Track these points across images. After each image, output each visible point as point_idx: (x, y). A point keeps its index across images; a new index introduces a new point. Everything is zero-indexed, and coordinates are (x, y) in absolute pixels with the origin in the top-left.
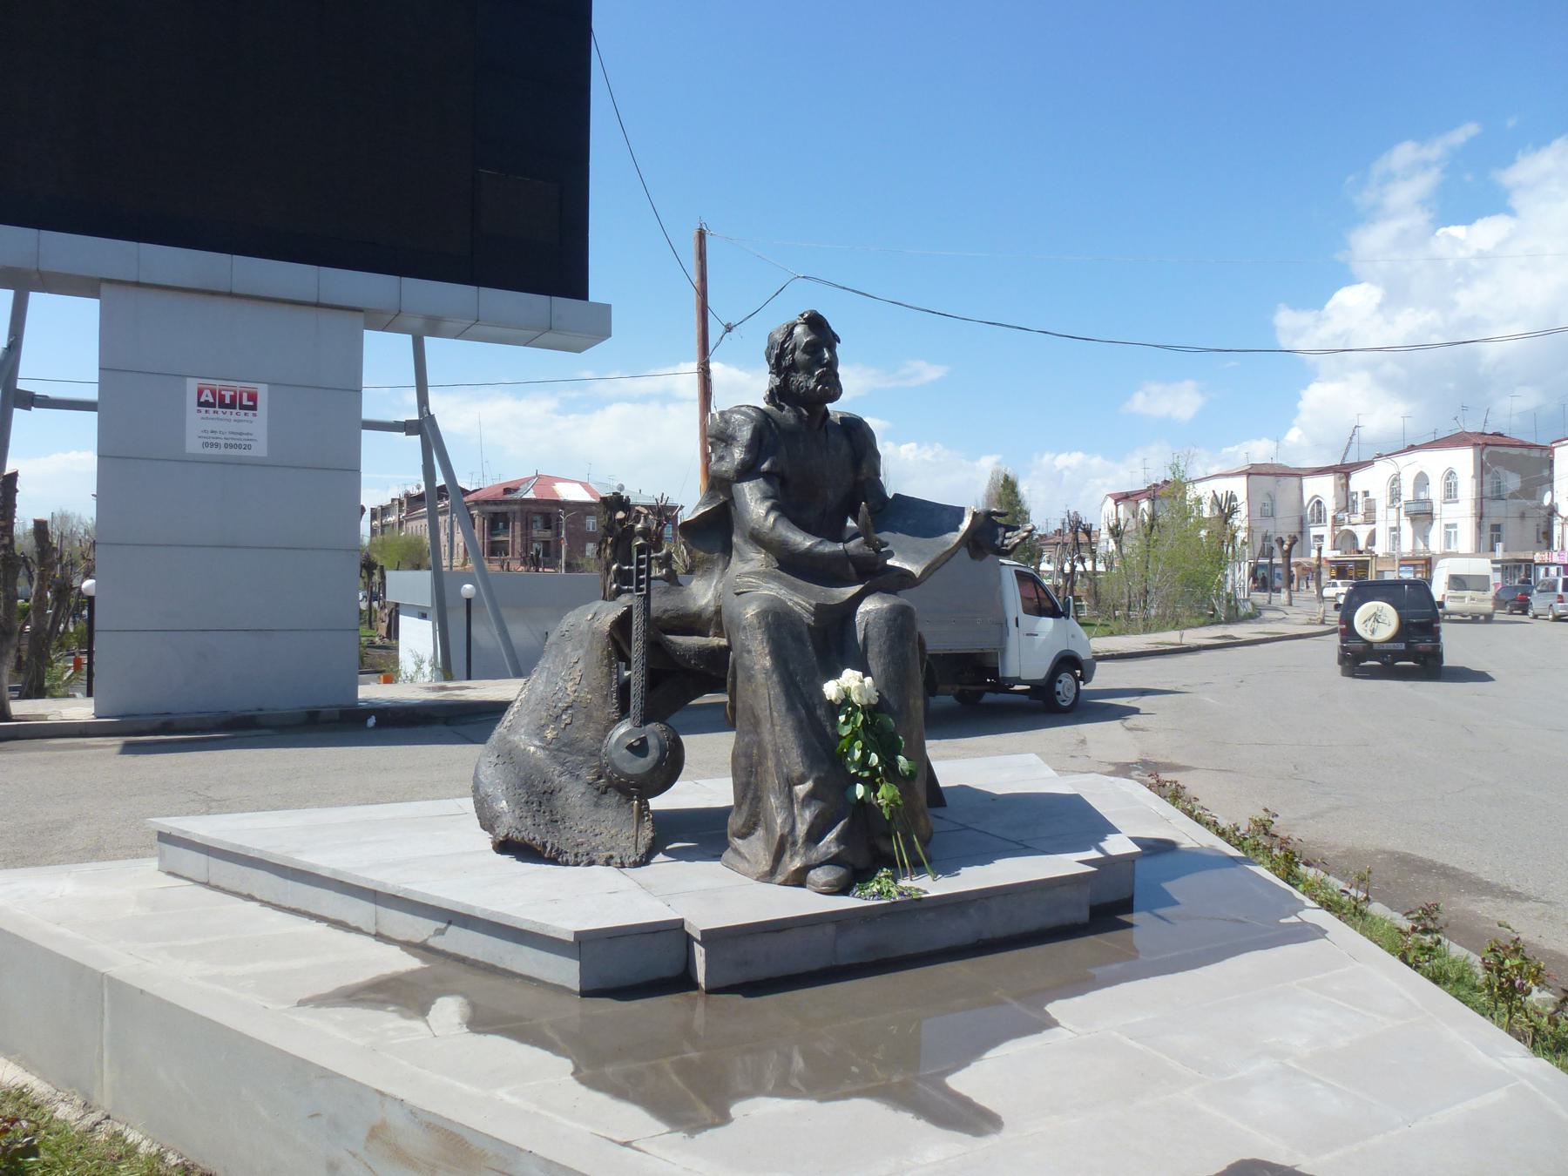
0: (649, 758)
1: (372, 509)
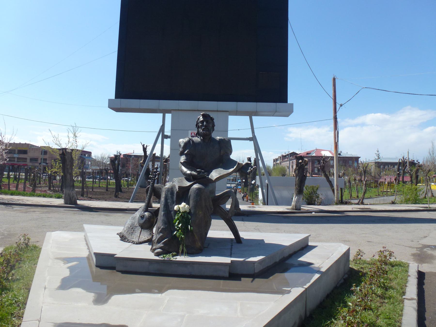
1: (274, 159)
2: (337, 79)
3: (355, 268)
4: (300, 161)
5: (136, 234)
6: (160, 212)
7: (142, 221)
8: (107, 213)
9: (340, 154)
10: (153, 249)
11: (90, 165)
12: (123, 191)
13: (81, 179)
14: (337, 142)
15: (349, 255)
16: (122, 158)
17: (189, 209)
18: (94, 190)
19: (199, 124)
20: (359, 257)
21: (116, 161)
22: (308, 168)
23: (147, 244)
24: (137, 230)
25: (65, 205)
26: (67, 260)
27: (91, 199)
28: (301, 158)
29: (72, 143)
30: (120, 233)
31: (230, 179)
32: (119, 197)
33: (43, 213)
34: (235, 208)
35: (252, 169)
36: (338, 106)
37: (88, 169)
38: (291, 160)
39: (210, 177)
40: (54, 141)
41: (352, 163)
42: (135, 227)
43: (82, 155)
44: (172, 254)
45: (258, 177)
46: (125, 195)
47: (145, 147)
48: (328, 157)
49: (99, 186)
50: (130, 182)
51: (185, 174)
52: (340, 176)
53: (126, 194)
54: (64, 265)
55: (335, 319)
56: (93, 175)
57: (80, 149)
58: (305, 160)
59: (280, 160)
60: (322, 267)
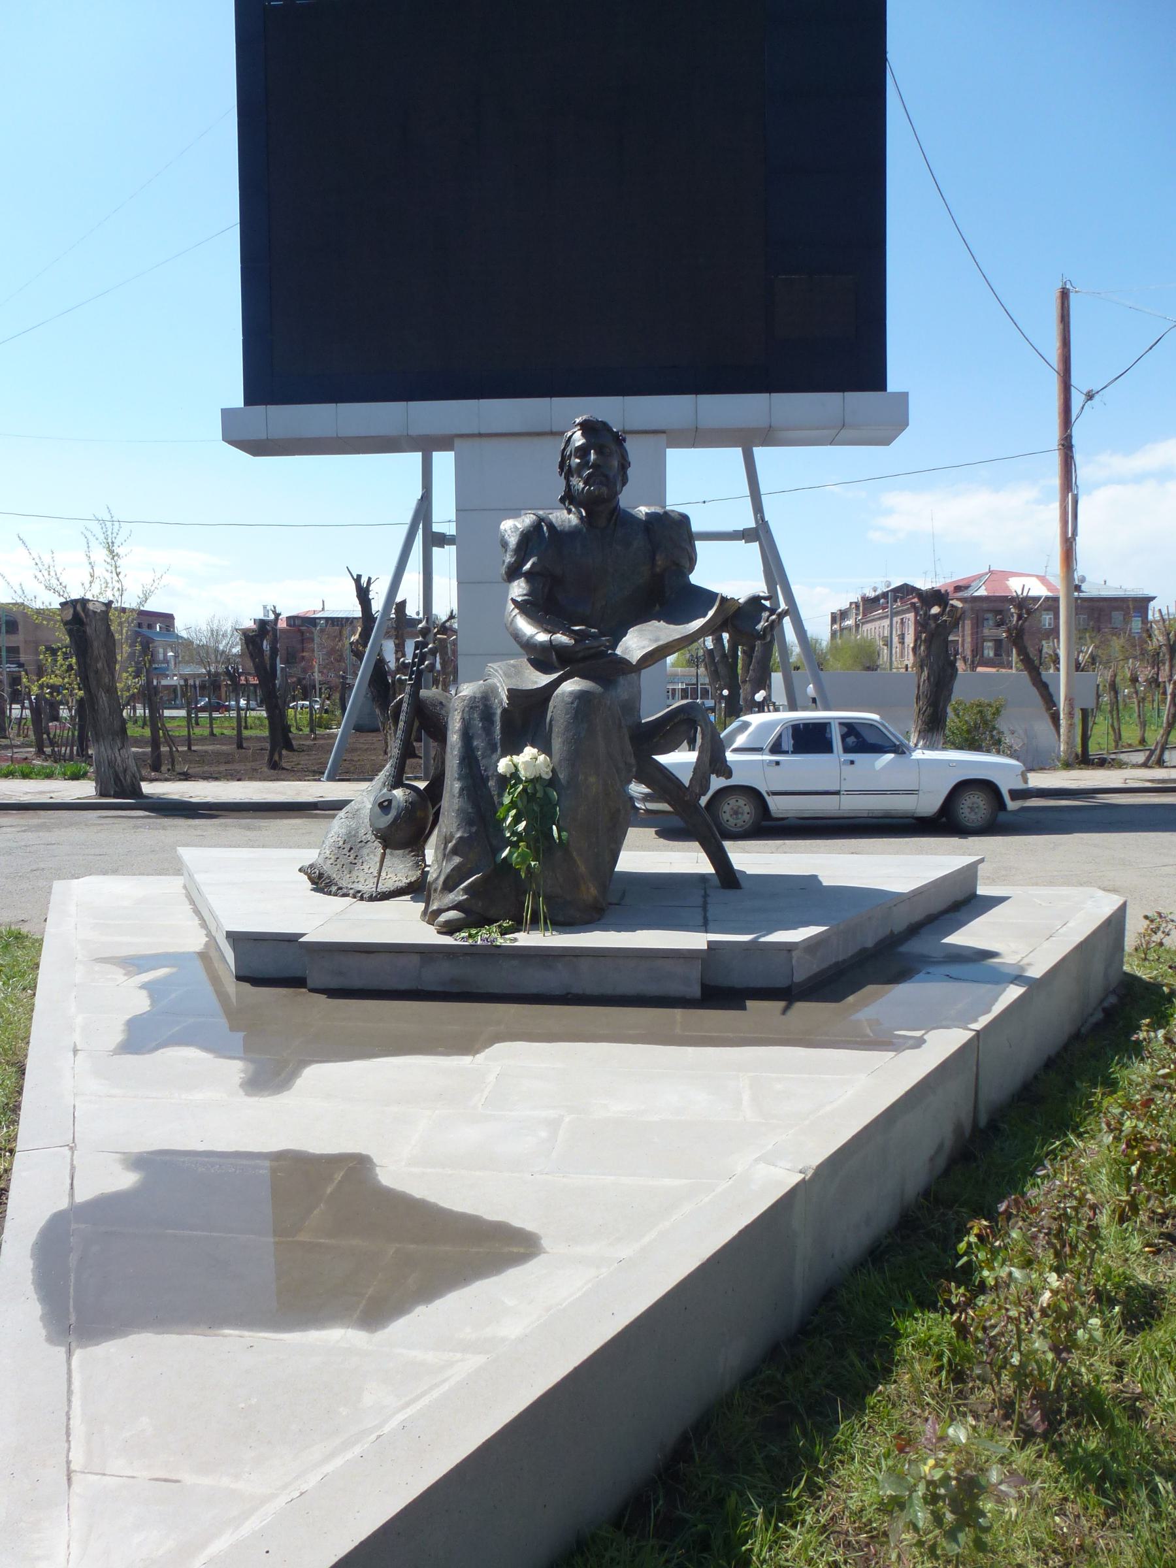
0: (390, 816)
1: (832, 613)
2: (1076, 292)
3: (1145, 974)
4: (935, 610)
5: (365, 867)
6: (447, 782)
7: (386, 820)
8: (248, 820)
9: (1078, 588)
10: (430, 910)
11: (173, 663)
12: (295, 747)
13: (147, 711)
14: (1070, 536)
15: (1124, 925)
16: (282, 630)
17: (549, 770)
18: (193, 748)
19: (573, 458)
20: (1156, 938)
21: (265, 643)
22: (960, 642)
23: (408, 897)
24: (368, 855)
25: (99, 799)
26: (134, 964)
27: (186, 777)
28: (937, 597)
29: (103, 581)
30: (311, 866)
31: (674, 690)
32: (283, 769)
33: (29, 829)
34: (710, 765)
35: (774, 617)
36: (1077, 400)
37: (167, 676)
38: (897, 613)
39: (619, 651)
40: (39, 575)
41: (1124, 619)
42: (360, 845)
43: (140, 625)
44: (500, 926)
45: (777, 678)
46: (304, 760)
47: (365, 586)
48: (1036, 599)
49: (212, 734)
50: (318, 716)
51: (528, 646)
52: (1080, 664)
53: (307, 758)
54: (126, 978)
55: (1080, 1136)
56: (185, 694)
57: (134, 605)
58: (952, 606)
59: (857, 614)
60: (1029, 964)
